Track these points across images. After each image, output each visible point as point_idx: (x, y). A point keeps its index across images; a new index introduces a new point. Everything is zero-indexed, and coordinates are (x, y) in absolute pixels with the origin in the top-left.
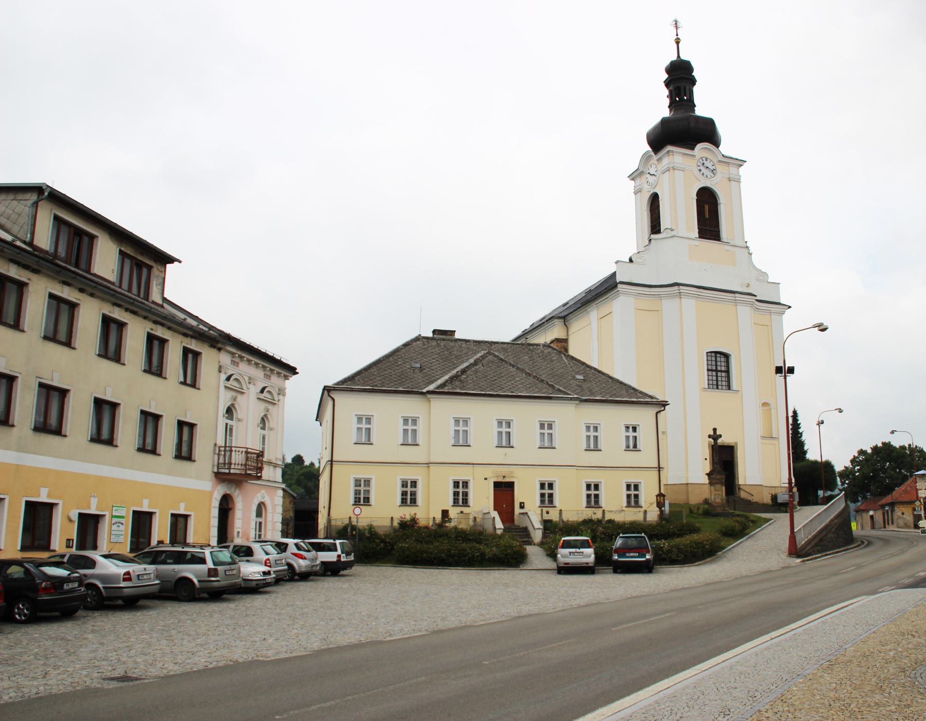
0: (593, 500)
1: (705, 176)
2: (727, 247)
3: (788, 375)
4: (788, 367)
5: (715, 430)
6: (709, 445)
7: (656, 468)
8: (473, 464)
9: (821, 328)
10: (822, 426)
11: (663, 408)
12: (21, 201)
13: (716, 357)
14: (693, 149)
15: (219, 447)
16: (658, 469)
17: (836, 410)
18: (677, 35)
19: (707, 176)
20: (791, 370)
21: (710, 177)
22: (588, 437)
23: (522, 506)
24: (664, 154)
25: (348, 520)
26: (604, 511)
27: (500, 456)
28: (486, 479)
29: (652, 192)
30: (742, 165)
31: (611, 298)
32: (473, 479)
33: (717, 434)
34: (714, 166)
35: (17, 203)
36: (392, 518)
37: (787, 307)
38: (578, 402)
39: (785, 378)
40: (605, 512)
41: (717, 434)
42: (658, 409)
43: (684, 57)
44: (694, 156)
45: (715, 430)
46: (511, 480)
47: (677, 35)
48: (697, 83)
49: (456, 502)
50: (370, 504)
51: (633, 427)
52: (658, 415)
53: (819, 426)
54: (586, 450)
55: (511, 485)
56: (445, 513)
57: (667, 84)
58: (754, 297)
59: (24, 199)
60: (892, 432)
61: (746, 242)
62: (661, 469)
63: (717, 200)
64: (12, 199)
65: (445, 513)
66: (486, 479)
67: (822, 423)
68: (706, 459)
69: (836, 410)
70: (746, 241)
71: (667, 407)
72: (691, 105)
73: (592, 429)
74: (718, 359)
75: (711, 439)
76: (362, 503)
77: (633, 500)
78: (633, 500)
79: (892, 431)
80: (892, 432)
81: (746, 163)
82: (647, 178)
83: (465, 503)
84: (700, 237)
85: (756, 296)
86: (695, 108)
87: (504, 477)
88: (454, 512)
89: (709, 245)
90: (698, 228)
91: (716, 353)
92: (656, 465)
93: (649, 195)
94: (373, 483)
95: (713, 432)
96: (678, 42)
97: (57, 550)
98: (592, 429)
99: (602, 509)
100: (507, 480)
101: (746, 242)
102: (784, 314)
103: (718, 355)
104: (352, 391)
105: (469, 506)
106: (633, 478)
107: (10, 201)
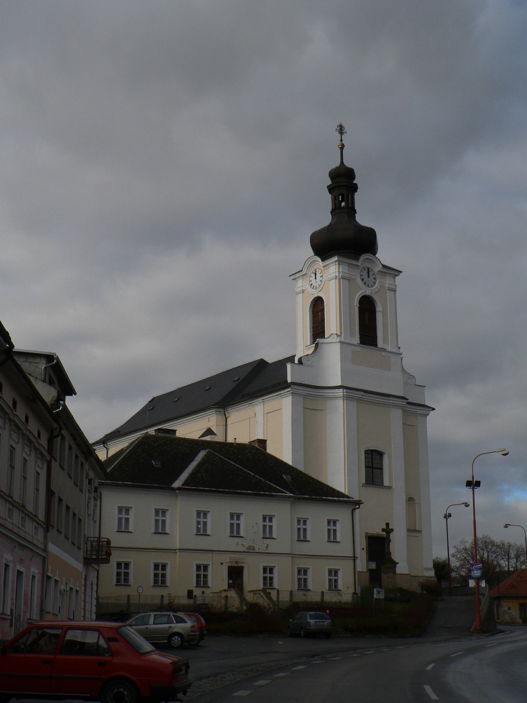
0: (303, 585)
1: (367, 285)
2: (384, 354)
3: (476, 487)
4: (476, 481)
5: (388, 525)
6: (366, 536)
7: (352, 557)
8: (212, 551)
9: (504, 453)
10: (449, 519)
11: (358, 506)
12: (32, 363)
13: (372, 454)
14: (358, 260)
15: (87, 538)
16: (353, 558)
17: (462, 504)
18: (341, 141)
19: (368, 285)
20: (478, 484)
21: (371, 286)
22: (299, 529)
23: (474, 586)
24: (332, 263)
25: (126, 598)
26: (57, 615)
27: (233, 544)
28: (222, 564)
29: (316, 296)
30: (398, 275)
31: (281, 396)
32: (212, 564)
33: (390, 528)
34: (374, 275)
35: (29, 364)
36: (323, 593)
37: (432, 409)
38: (293, 500)
39: (473, 490)
40: (325, 594)
41: (390, 528)
42: (353, 507)
43: (348, 164)
44: (358, 266)
45: (388, 525)
46: (242, 565)
47: (341, 141)
48: (358, 190)
49: (198, 585)
50: (166, 585)
51: (269, 518)
52: (354, 512)
53: (447, 520)
54: (196, 534)
55: (241, 569)
56: (190, 593)
57: (331, 189)
58: (406, 401)
59: (34, 362)
60: (506, 526)
61: (399, 348)
62: (356, 558)
63: (375, 307)
64: (24, 360)
65: (190, 593)
66: (222, 564)
67: (450, 515)
68: (363, 549)
69: (462, 504)
70: (399, 346)
71: (361, 505)
72: (351, 211)
73: (302, 522)
74: (374, 456)
75: (384, 532)
76: (123, 583)
77: (333, 585)
78: (333, 585)
79: (506, 525)
80: (506, 526)
81: (401, 273)
82: (311, 281)
83: (206, 585)
84: (362, 343)
85: (408, 400)
86: (356, 215)
87: (236, 562)
88: (197, 592)
89: (368, 351)
90: (360, 334)
91: (372, 451)
92: (352, 555)
93: (313, 298)
94: (131, 567)
95: (385, 526)
96: (342, 147)
97: (311, 589)
98: (302, 522)
99: (58, 613)
100: (239, 565)
101: (399, 348)
102: (428, 415)
103: (374, 453)
104: (117, 486)
105: (208, 587)
106: (333, 565)
107: (22, 362)
